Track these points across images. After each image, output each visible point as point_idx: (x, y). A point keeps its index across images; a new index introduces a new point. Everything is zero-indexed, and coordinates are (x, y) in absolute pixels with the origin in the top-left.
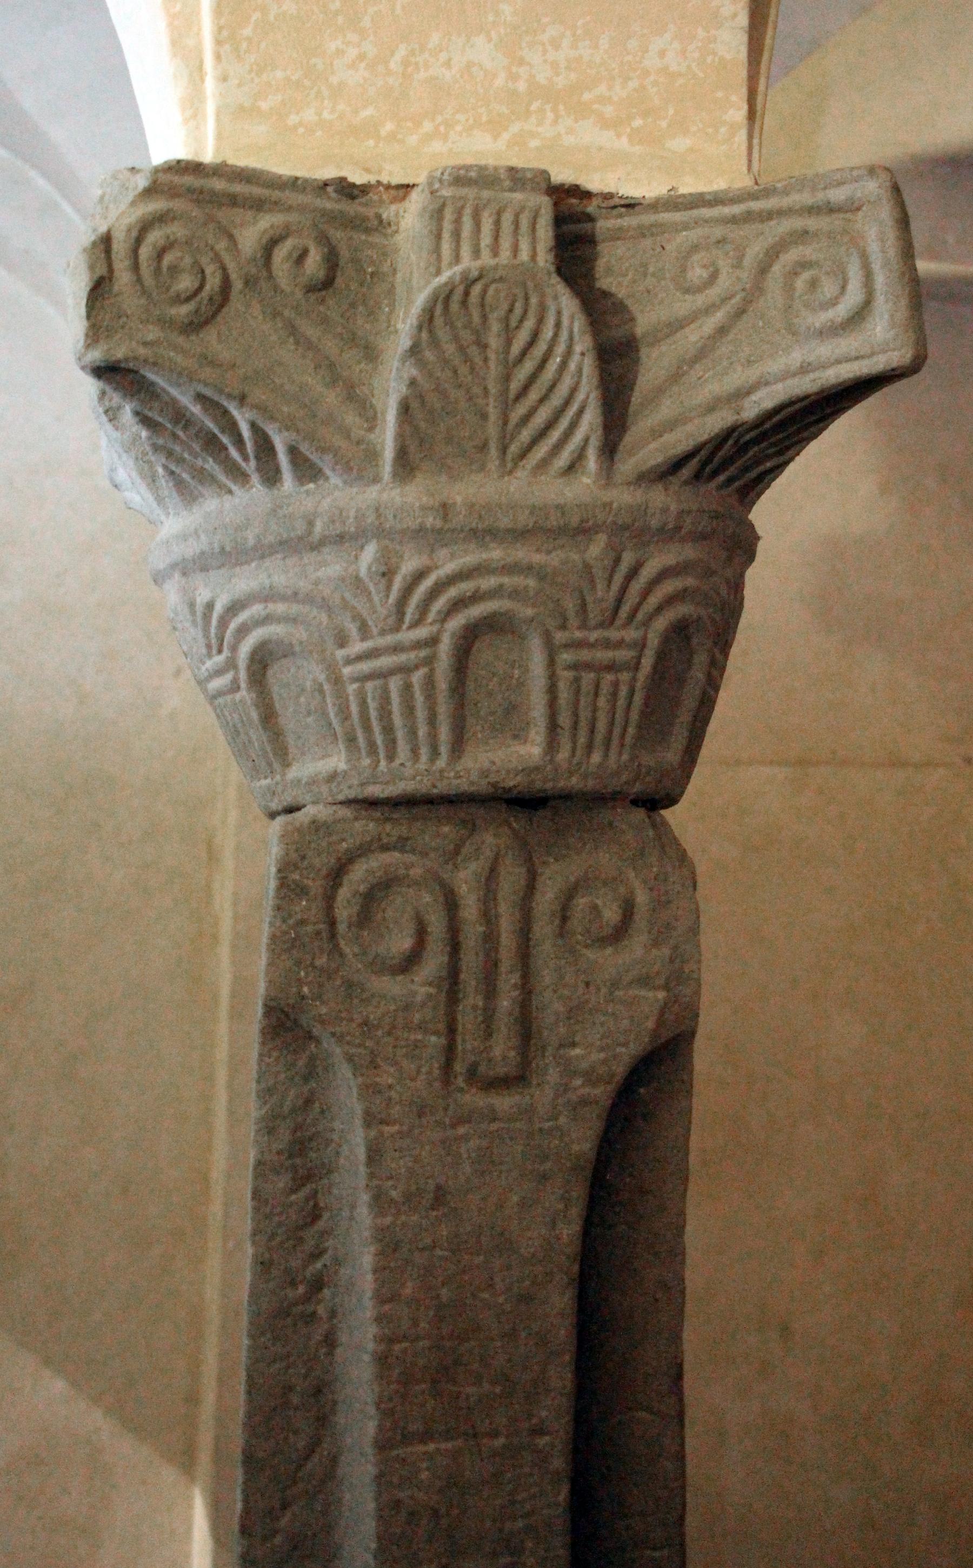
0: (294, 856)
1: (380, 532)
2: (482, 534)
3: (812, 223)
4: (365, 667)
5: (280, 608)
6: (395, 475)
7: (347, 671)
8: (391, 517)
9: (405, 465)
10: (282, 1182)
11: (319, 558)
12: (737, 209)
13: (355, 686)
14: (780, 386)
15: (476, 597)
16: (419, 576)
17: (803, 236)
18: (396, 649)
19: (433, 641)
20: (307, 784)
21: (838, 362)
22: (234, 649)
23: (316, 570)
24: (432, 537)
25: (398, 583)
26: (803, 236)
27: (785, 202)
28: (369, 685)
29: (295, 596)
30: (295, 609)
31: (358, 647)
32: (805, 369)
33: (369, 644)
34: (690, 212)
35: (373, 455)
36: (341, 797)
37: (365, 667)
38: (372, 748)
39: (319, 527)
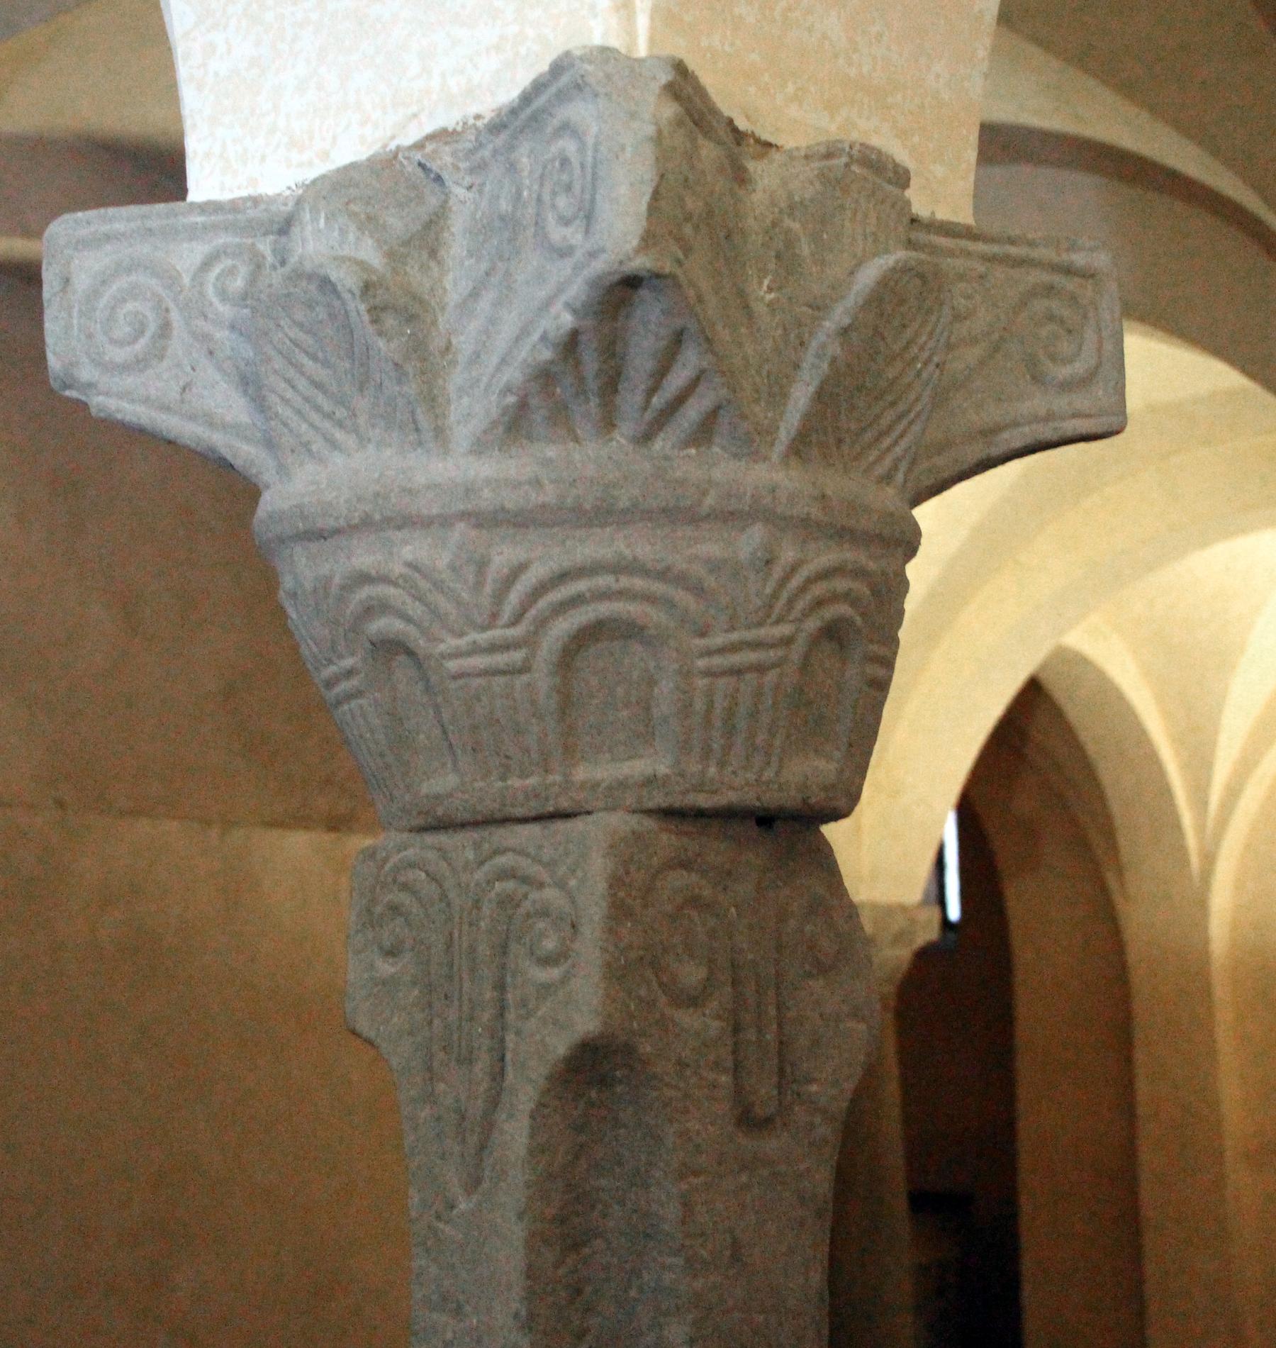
0: (621, 871)
1: (770, 517)
2: (843, 534)
3: (1058, 279)
4: (718, 661)
5: (638, 583)
6: (786, 457)
7: (701, 663)
8: (784, 500)
9: (799, 447)
10: (549, 1256)
11: (696, 534)
12: (995, 249)
13: (706, 681)
14: (1027, 429)
15: (576, 601)
16: (794, 569)
17: (1050, 290)
18: (757, 645)
19: (787, 641)
20: (610, 788)
21: (1074, 416)
22: (542, 623)
23: (689, 546)
24: (807, 528)
25: (777, 572)
26: (1050, 290)
27: (1036, 254)
28: (722, 682)
29: (663, 575)
30: (658, 587)
31: (719, 640)
32: (1050, 417)
33: (735, 636)
34: (958, 241)
35: (769, 432)
36: (650, 805)
37: (718, 661)
38: (707, 753)
39: (709, 501)
